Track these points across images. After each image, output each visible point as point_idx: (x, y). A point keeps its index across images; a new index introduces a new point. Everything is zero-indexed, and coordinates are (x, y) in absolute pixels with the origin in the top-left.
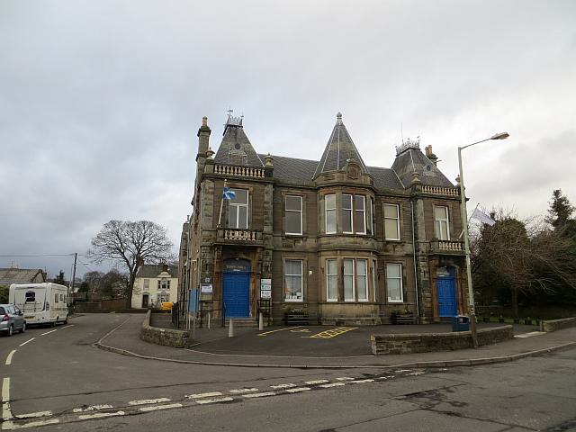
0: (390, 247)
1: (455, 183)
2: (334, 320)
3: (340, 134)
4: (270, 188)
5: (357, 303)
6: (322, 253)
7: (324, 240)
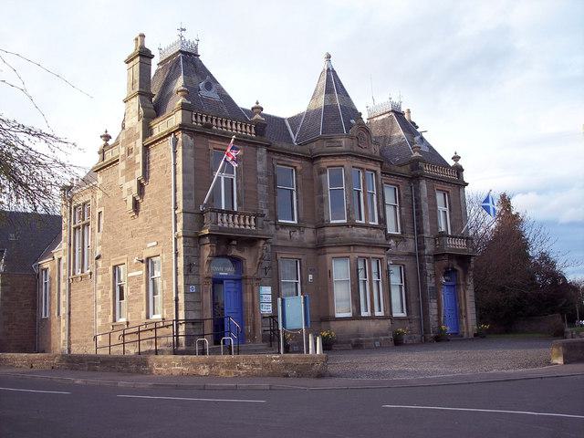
0: (392, 242)
1: (452, 163)
2: (350, 342)
3: (332, 84)
4: (262, 152)
5: (373, 318)
6: (328, 250)
7: (329, 232)
